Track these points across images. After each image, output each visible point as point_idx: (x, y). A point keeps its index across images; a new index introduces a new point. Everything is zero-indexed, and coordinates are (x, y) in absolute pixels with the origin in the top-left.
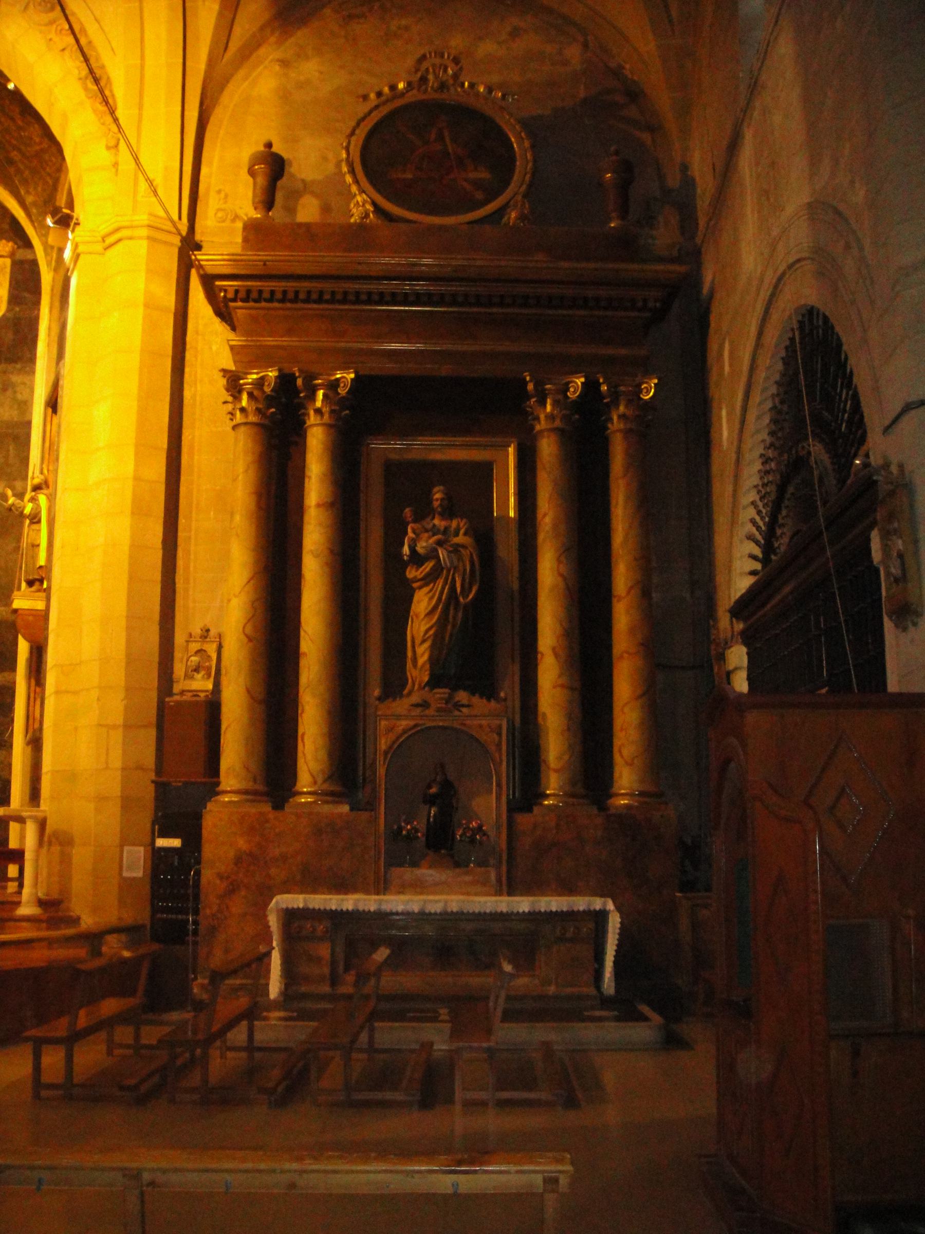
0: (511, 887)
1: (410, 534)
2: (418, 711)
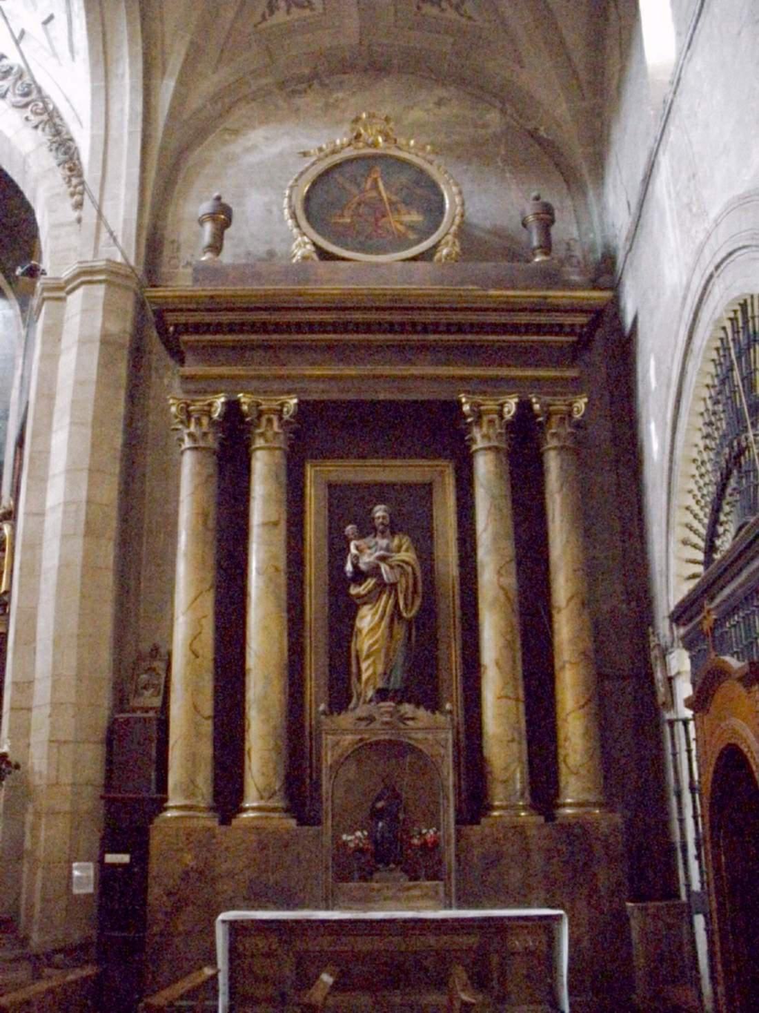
0: (465, 900)
1: (353, 550)
2: (363, 725)
